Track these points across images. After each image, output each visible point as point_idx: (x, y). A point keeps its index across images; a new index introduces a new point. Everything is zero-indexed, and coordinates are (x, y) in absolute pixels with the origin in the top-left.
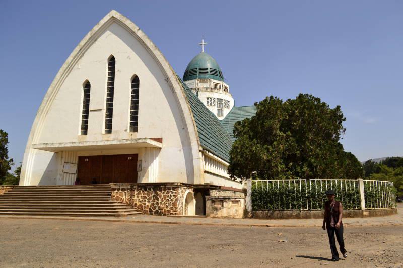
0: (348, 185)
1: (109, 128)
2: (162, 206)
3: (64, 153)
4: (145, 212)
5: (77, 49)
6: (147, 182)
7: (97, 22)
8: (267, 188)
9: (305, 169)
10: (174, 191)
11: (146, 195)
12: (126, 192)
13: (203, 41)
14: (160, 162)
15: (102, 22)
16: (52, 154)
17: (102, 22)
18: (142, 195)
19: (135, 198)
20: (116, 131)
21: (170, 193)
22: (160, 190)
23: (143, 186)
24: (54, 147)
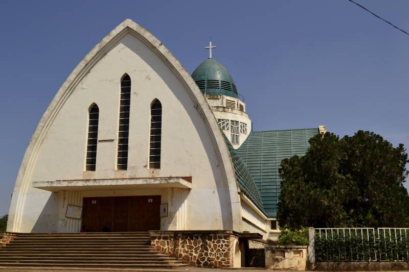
0: (387, 235)
1: (123, 163)
2: (211, 257)
3: (66, 192)
4: (192, 264)
5: (82, 64)
7: (108, 33)
8: (331, 238)
9: (370, 216)
10: (226, 241)
11: (193, 245)
12: (169, 240)
13: (211, 43)
14: (189, 207)
15: (115, 32)
16: (50, 193)
17: (115, 32)
18: (188, 244)
19: (180, 247)
20: (133, 167)
21: (221, 243)
22: (210, 239)
23: (189, 234)
24: (62, 186)
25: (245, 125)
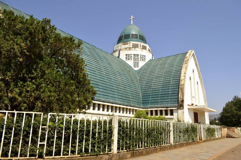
13: (132, 16)
25: (144, 56)
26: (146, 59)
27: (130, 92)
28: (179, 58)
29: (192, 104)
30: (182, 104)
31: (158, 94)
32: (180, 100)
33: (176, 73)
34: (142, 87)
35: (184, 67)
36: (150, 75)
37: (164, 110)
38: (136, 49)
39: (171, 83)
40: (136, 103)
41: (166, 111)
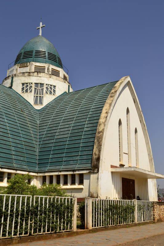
6: (76, 181)
13: (41, 23)
25: (52, 87)
26: (56, 92)
27: (15, 145)
28: (104, 89)
29: (122, 166)
30: (96, 165)
31: (62, 147)
32: (95, 157)
33: (94, 112)
34: (41, 137)
35: (107, 103)
36: (57, 117)
37: (48, 175)
38: (39, 75)
39: (85, 129)
40: (23, 163)
41: (73, 176)
